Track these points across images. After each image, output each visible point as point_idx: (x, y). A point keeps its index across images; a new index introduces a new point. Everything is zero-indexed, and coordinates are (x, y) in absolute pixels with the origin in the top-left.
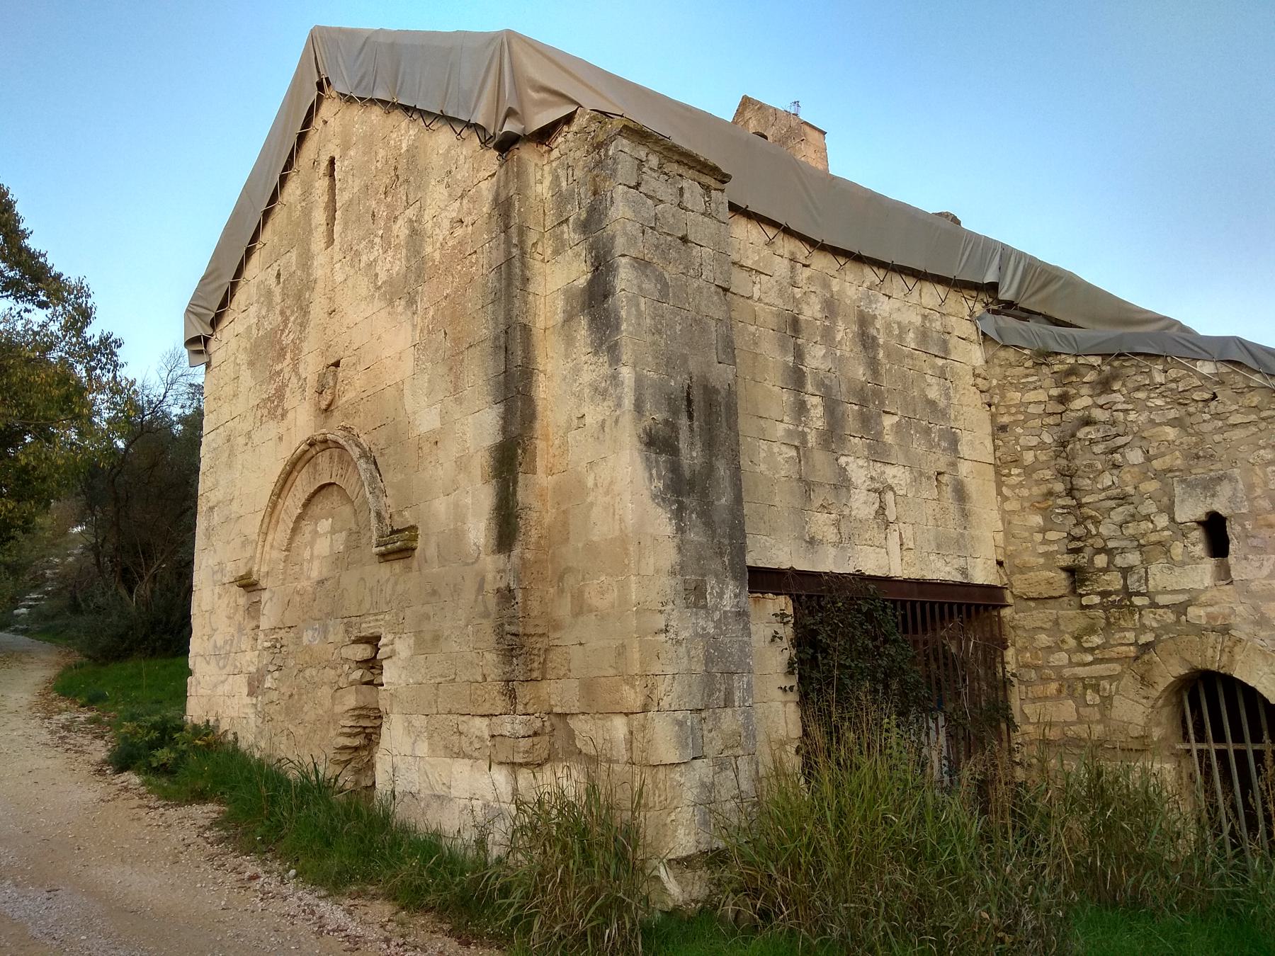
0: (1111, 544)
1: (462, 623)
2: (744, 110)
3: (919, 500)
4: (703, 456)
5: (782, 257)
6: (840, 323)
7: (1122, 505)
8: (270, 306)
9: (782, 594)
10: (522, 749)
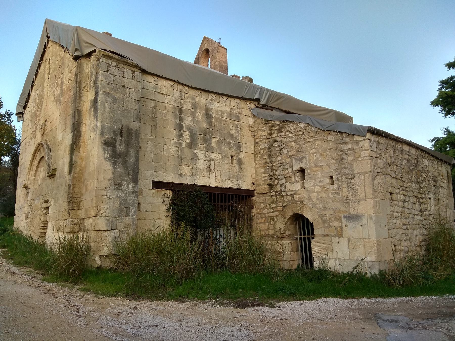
0: (279, 177)
2: (204, 41)
5: (177, 90)
6: (198, 110)
7: (282, 166)
9: (168, 189)
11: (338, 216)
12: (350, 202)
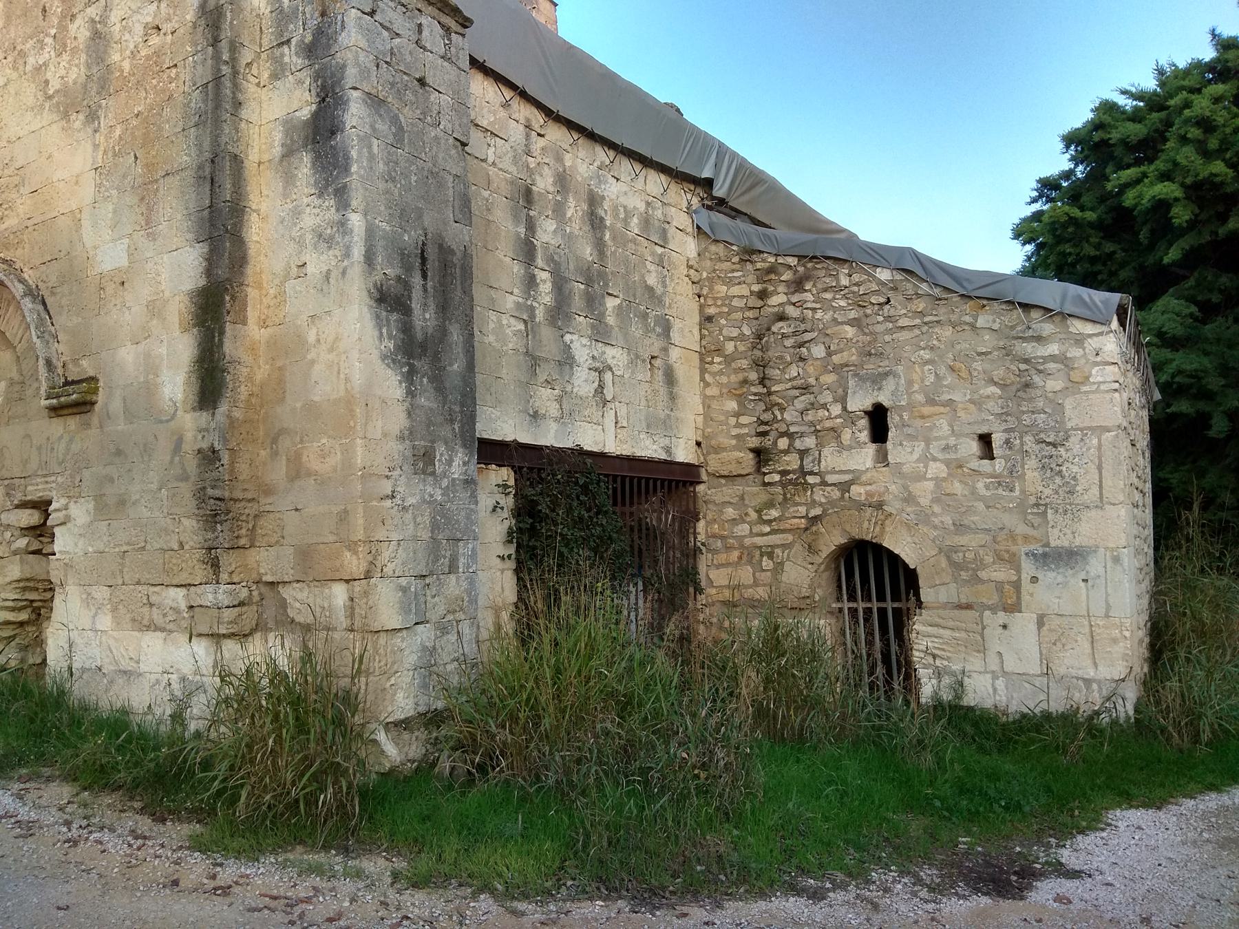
0: (792, 429)
1: (154, 486)
3: (634, 382)
4: (437, 319)
5: (517, 122)
6: (571, 200)
9: (504, 466)
10: (226, 620)
11: (1008, 552)
12: (1049, 511)
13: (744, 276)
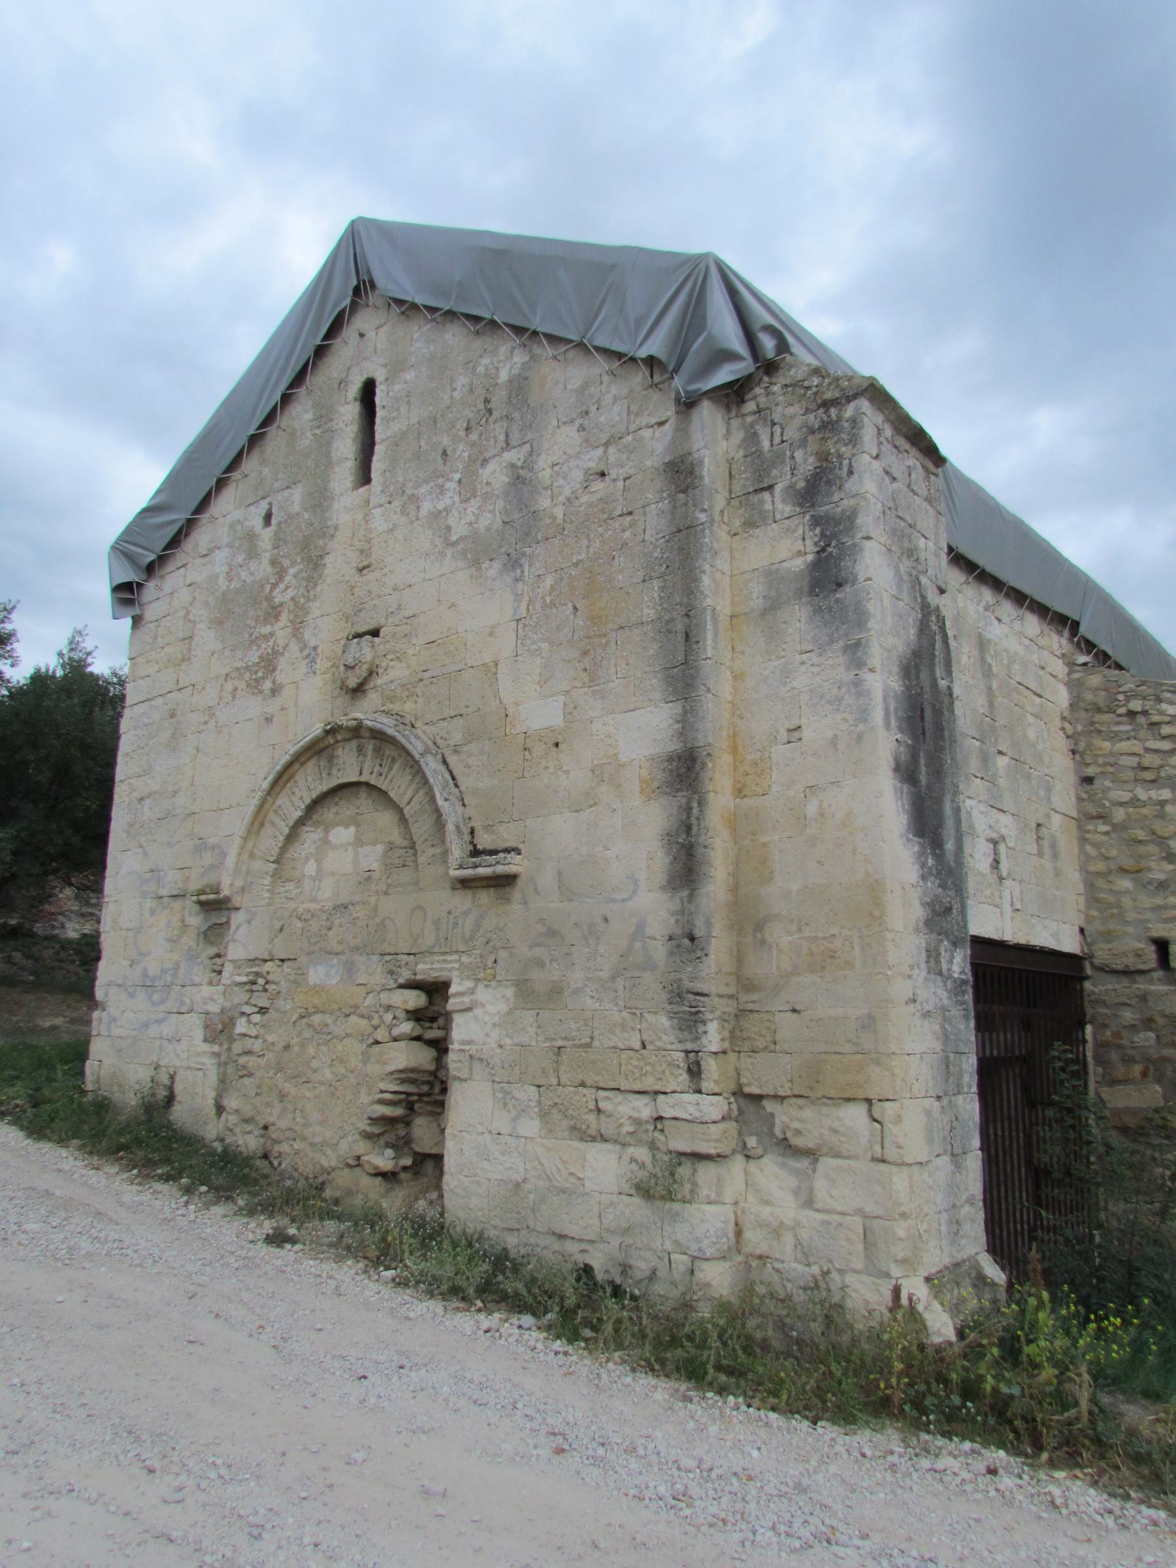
1: (604, 975)
8: (253, 553)
13: (1134, 730)
